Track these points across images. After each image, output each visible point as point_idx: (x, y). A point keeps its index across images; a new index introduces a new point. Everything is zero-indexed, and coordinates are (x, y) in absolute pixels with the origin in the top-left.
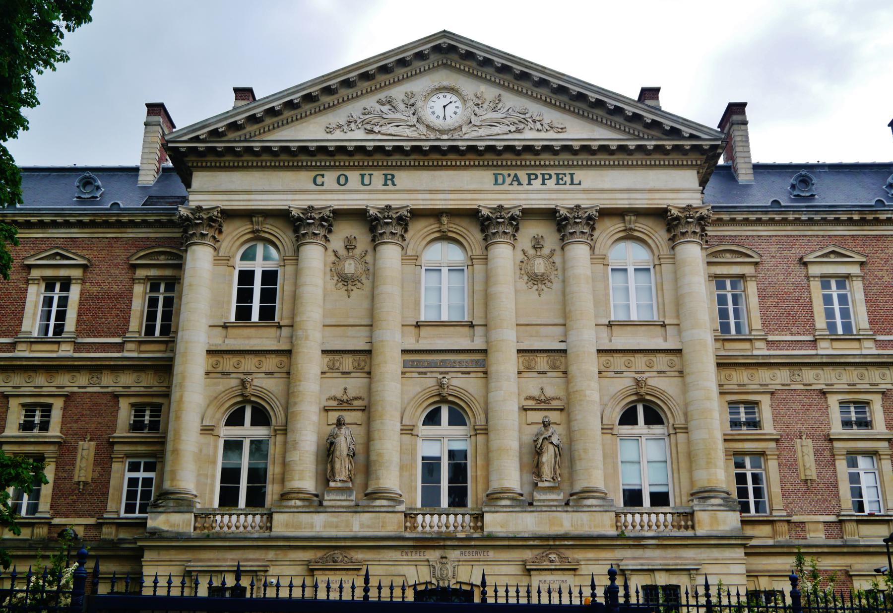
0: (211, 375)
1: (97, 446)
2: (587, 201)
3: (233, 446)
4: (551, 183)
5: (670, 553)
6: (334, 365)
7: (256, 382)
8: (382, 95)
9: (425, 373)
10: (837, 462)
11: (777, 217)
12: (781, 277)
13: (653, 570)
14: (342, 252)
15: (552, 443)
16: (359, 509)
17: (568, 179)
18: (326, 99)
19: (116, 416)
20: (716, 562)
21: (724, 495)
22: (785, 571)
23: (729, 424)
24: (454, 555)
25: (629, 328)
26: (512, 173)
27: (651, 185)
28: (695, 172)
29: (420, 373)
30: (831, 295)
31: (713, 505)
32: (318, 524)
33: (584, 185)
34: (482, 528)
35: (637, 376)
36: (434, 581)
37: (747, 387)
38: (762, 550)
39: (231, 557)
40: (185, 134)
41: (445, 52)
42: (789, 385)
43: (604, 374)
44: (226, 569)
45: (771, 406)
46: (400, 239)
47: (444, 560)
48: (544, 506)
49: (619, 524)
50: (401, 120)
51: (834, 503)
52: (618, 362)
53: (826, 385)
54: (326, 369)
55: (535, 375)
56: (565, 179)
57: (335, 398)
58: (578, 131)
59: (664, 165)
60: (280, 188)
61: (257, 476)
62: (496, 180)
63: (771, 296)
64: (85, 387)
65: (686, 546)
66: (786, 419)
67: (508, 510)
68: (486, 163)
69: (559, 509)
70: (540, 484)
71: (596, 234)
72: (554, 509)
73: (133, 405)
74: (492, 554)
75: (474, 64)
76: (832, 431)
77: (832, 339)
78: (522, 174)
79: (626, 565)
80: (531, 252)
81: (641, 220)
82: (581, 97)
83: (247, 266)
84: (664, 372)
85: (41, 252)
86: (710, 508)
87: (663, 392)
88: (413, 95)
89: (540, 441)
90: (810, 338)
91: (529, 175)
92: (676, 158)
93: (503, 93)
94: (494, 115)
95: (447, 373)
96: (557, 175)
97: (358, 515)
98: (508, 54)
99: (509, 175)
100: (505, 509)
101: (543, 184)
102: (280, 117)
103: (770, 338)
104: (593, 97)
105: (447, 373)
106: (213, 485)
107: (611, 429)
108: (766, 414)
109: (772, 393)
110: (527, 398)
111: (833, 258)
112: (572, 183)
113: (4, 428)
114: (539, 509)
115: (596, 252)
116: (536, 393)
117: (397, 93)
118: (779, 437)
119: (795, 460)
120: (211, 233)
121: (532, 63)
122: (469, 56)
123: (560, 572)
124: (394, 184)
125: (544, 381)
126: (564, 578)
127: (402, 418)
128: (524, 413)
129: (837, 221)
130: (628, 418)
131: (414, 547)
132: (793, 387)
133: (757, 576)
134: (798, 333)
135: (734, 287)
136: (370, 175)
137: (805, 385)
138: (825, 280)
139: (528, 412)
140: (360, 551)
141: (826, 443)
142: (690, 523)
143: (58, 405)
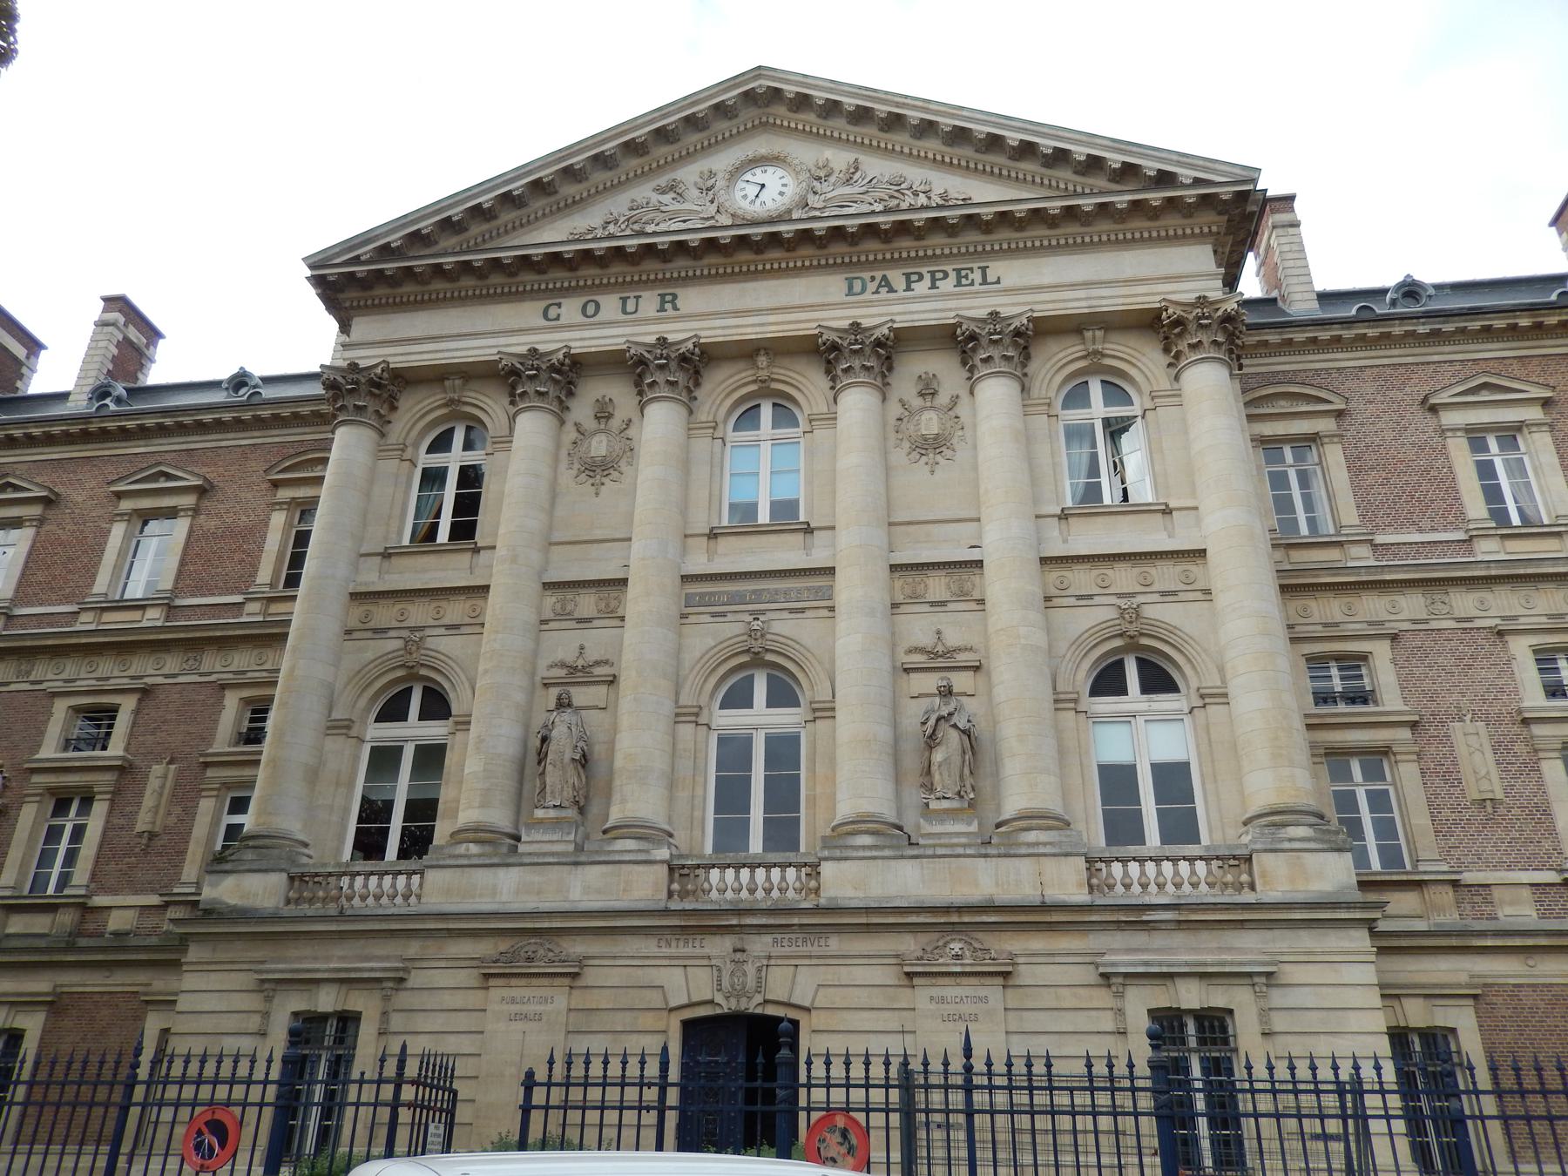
0: (356, 635)
1: (180, 772)
2: (1014, 308)
3: (384, 760)
4: (947, 285)
5: (1207, 939)
6: (563, 608)
7: (430, 643)
8: (663, 181)
9: (723, 614)
10: (1545, 765)
11: (1372, 332)
12: (1389, 435)
13: (1171, 976)
14: (589, 424)
15: (955, 726)
16: (583, 858)
17: (977, 276)
18: (569, 190)
19: (216, 721)
20: (1309, 959)
21: (1313, 820)
22: (1460, 986)
23: (1311, 698)
24: (760, 945)
25: (1100, 519)
26: (878, 275)
27: (1129, 273)
28: (1208, 249)
29: (714, 615)
30: (1492, 462)
31: (1290, 840)
32: (505, 889)
33: (1005, 283)
34: (817, 891)
35: (1122, 603)
36: (719, 999)
37: (1342, 627)
38: (1404, 943)
39: (341, 953)
40: (338, 255)
41: (764, 104)
42: (1426, 621)
43: (1056, 602)
44: (326, 976)
45: (1394, 661)
46: (684, 393)
47: (739, 956)
48: (941, 846)
49: (1094, 881)
50: (691, 212)
51: (1547, 845)
52: (1083, 579)
53: (1503, 618)
54: (548, 614)
55: (926, 608)
56: (971, 276)
57: (563, 665)
58: (985, 194)
59: (366, 306)
60: (490, 328)
61: (423, 810)
62: (850, 287)
63: (1372, 468)
64: (174, 676)
65: (1241, 924)
66: (1427, 684)
67: (868, 853)
68: (831, 261)
69: (969, 851)
70: (934, 805)
71: (1032, 367)
72: (960, 851)
73: (246, 701)
74: (835, 944)
75: (812, 117)
76: (1526, 704)
77: (1503, 536)
78: (896, 277)
79: (1113, 964)
80: (917, 402)
81: (1114, 337)
82: (994, 143)
83: (436, 460)
84: (1174, 593)
85: (135, 473)
86: (1287, 845)
87: (1173, 630)
88: (712, 174)
89: (932, 722)
90: (1461, 536)
91: (908, 276)
92: (1172, 222)
93: (862, 158)
94: (847, 190)
95: (763, 612)
96: (958, 271)
97: (580, 868)
98: (867, 89)
99: (873, 279)
100: (861, 854)
101: (933, 286)
102: (494, 223)
103: (1380, 539)
104: (1013, 138)
105: (763, 612)
106: (344, 828)
107: (1076, 701)
108: (1384, 673)
109: (1394, 638)
110: (909, 652)
111: (1485, 396)
112: (984, 282)
113: (40, 746)
114: (930, 852)
115: (1035, 392)
116: (927, 641)
117: (689, 174)
118: (1417, 718)
119: (1455, 763)
120: (372, 405)
121: (906, 97)
122: (802, 102)
123: (973, 980)
124: (675, 308)
125: (941, 620)
126: (982, 992)
127: (677, 694)
128: (905, 675)
129: (1487, 333)
130: (1108, 681)
131: (683, 929)
132: (1434, 625)
133: (1398, 996)
134: (1433, 529)
135: (1299, 458)
136: (637, 298)
137: (1459, 620)
138: (1476, 437)
139: (913, 675)
140: (579, 938)
141: (1516, 729)
142: (1245, 878)
143: (128, 704)
